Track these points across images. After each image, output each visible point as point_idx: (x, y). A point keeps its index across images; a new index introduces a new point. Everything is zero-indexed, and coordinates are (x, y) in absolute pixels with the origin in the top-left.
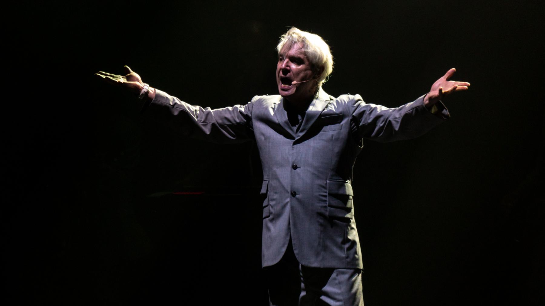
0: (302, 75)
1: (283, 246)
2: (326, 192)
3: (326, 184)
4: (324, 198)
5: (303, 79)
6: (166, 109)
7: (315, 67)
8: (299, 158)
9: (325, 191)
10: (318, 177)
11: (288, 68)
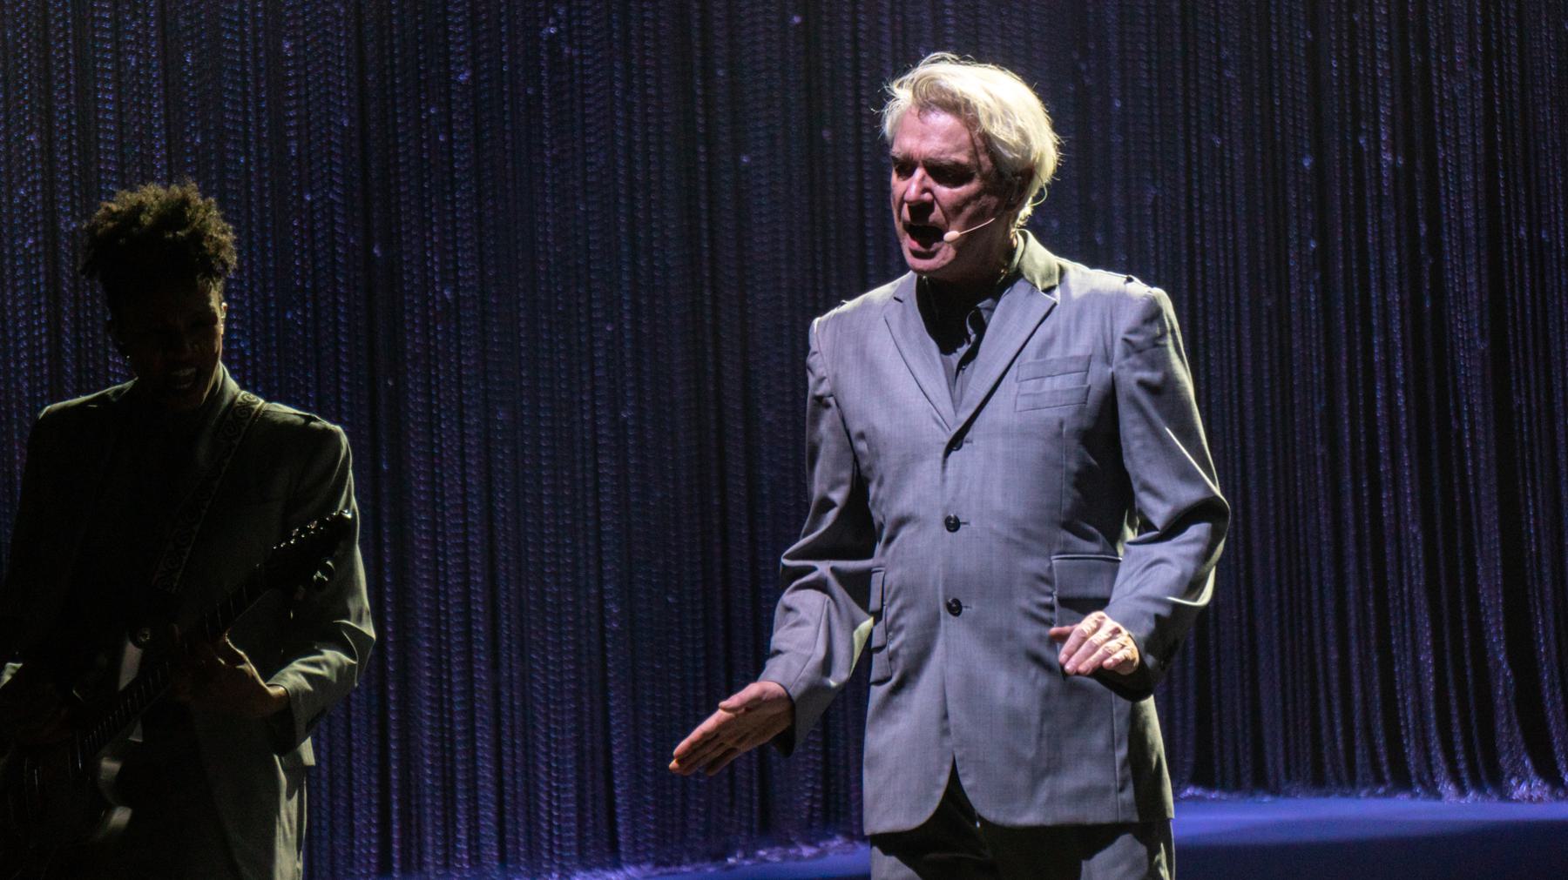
0: (969, 210)
1: (940, 772)
2: (1051, 595)
3: (1050, 569)
4: (1045, 614)
5: (971, 221)
6: (65, 409)
7: (1001, 177)
8: (963, 493)
9: (1049, 589)
10: (1026, 551)
11: (927, 196)
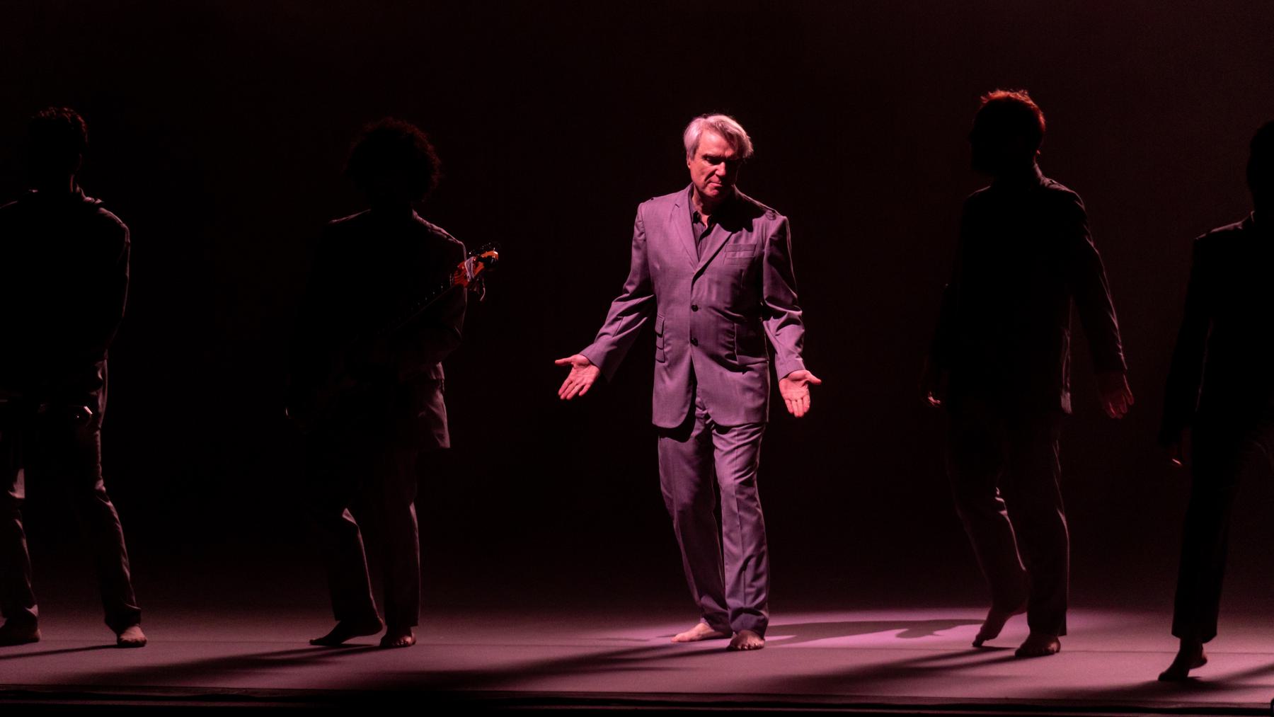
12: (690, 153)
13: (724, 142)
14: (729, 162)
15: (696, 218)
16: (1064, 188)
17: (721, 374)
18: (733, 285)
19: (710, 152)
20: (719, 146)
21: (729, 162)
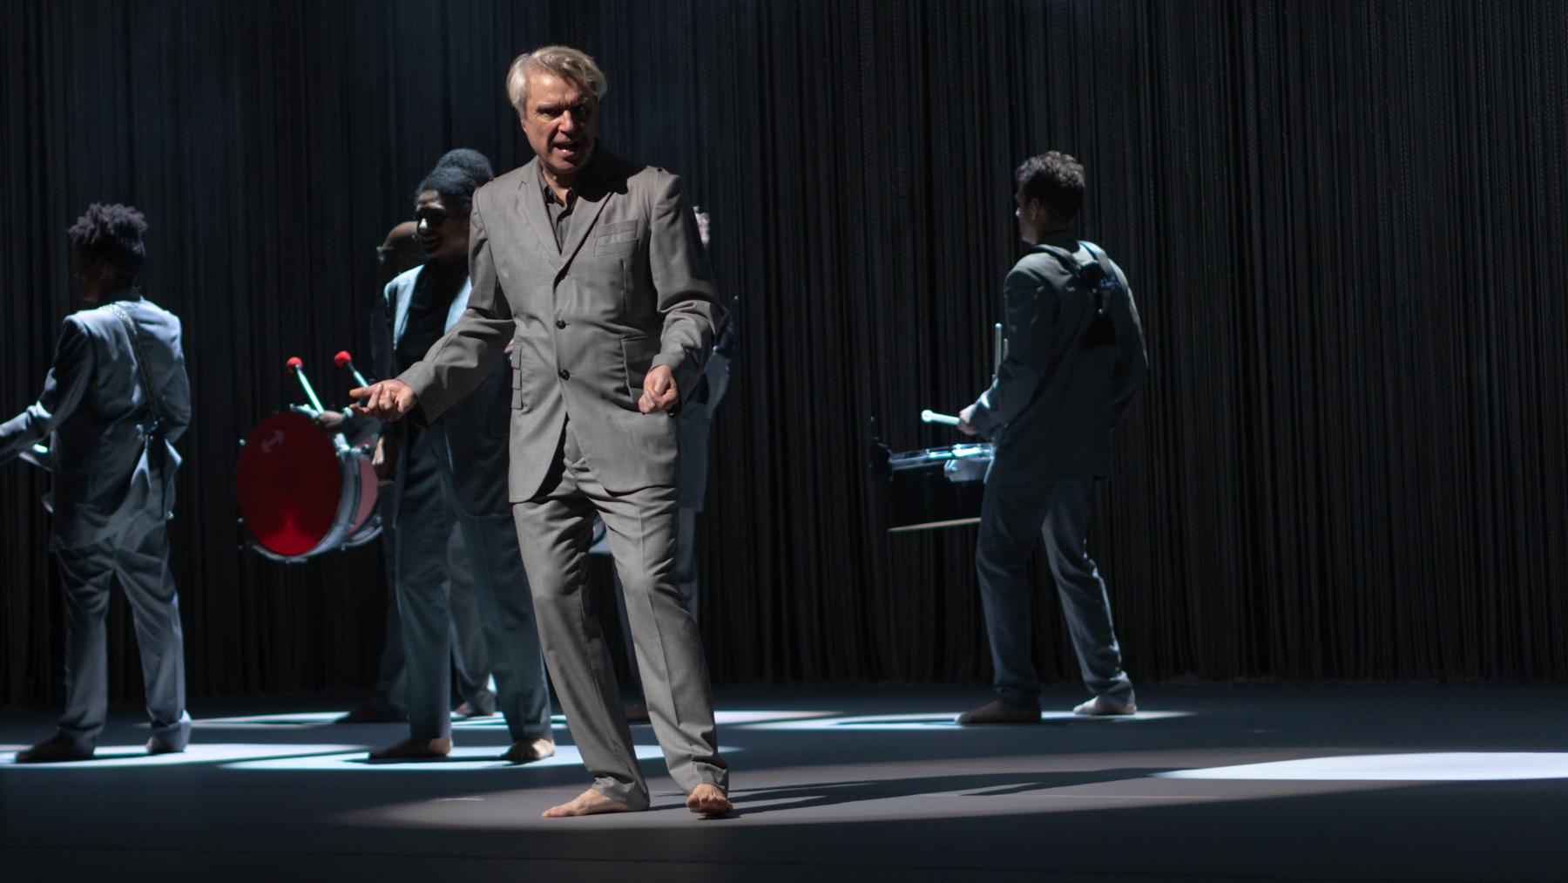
4: (620, 375)
12: (521, 111)
13: (560, 82)
14: (575, 110)
15: (549, 198)
16: (1137, 319)
17: (609, 418)
18: (612, 284)
19: (544, 103)
20: (554, 89)
21: (575, 110)
